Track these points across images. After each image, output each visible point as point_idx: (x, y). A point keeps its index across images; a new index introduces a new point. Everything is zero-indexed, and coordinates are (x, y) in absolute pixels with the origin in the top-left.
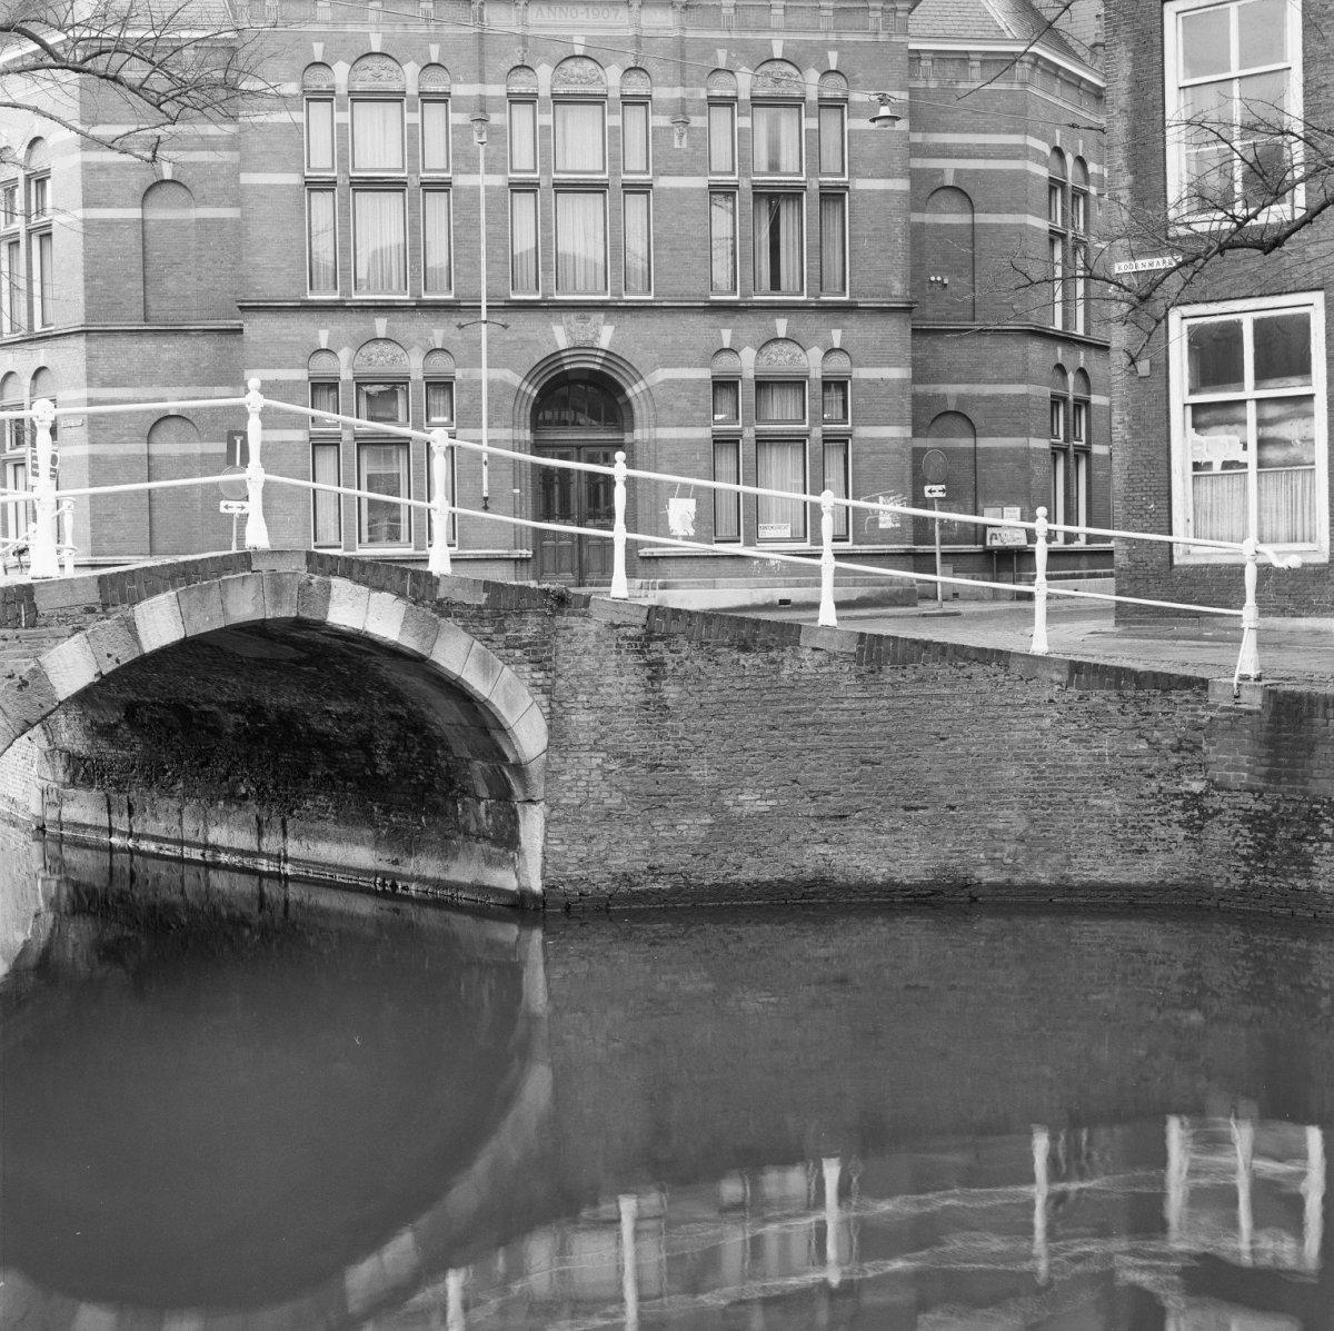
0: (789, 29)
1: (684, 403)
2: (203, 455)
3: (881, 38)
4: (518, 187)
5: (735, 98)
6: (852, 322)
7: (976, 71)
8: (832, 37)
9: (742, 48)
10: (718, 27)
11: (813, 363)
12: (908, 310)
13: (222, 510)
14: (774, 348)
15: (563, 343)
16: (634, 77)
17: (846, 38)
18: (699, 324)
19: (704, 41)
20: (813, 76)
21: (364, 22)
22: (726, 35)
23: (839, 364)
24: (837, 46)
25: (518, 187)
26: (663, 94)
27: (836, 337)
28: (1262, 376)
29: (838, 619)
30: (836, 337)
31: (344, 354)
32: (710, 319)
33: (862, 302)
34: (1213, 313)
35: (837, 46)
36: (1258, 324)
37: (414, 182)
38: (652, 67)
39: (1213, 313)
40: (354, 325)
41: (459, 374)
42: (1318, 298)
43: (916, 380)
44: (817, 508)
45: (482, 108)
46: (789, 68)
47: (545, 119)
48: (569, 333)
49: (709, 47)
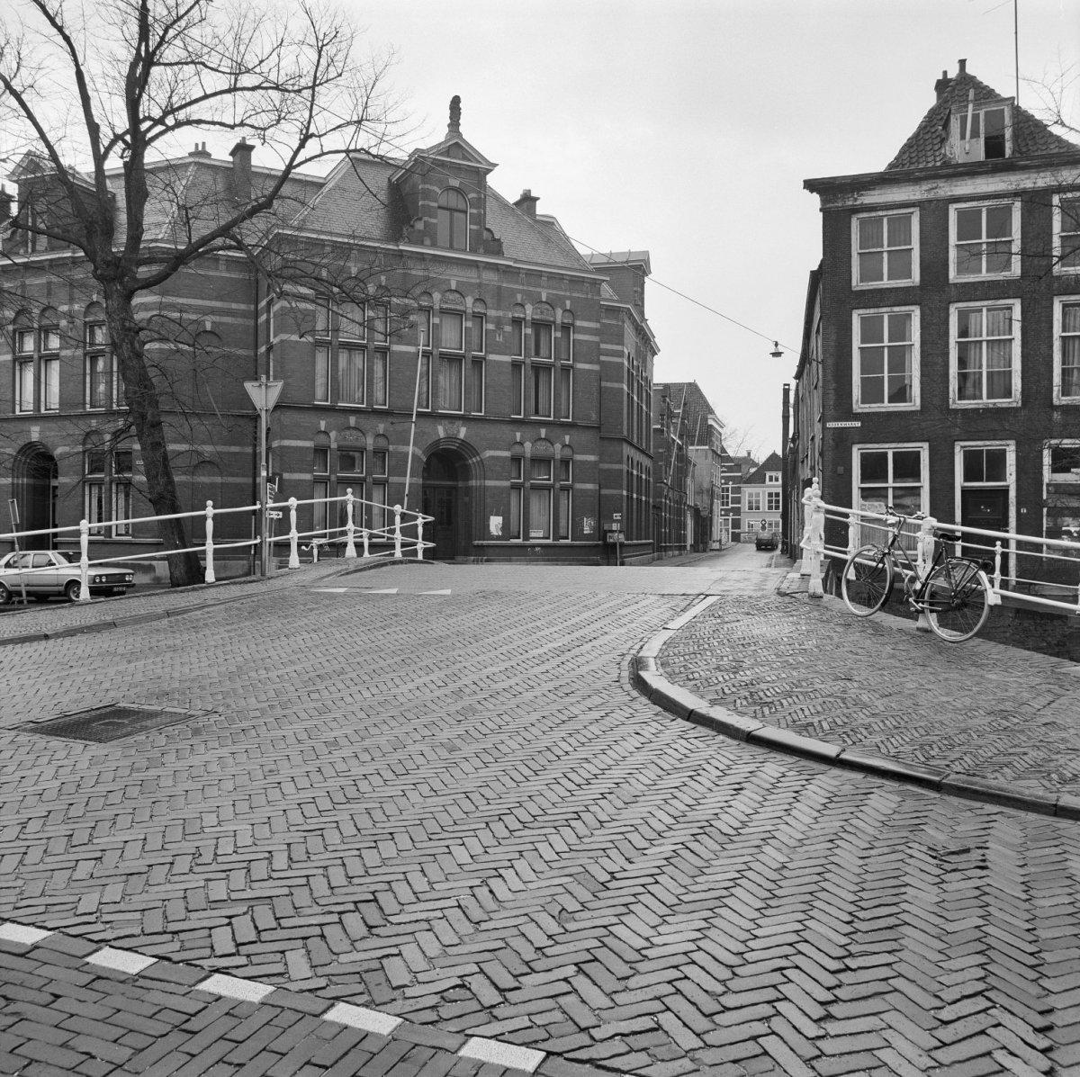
0: (549, 288)
1: (498, 468)
2: (211, 484)
3: (589, 296)
4: (318, 344)
5: (465, 312)
6: (573, 432)
7: (222, 267)
8: (568, 294)
9: (528, 294)
10: (517, 283)
11: (557, 450)
12: (599, 428)
13: (281, 513)
14: (539, 443)
15: (442, 434)
16: (478, 304)
17: (574, 295)
18: (506, 429)
19: (512, 290)
20: (559, 312)
21: (539, 286)
22: (521, 287)
23: (382, 442)
24: (569, 298)
25: (318, 344)
26: (492, 313)
27: (381, 428)
28: (897, 476)
29: (301, 562)
30: (381, 428)
31: (528, 445)
32: (510, 427)
33: (579, 422)
34: (874, 448)
35: (569, 298)
36: (894, 454)
37: (371, 346)
38: (488, 300)
39: (874, 448)
40: (339, 419)
41: (391, 448)
42: (926, 445)
43: (601, 461)
44: (369, 508)
45: (405, 313)
46: (547, 306)
47: (437, 320)
48: (445, 430)
49: (513, 292)
